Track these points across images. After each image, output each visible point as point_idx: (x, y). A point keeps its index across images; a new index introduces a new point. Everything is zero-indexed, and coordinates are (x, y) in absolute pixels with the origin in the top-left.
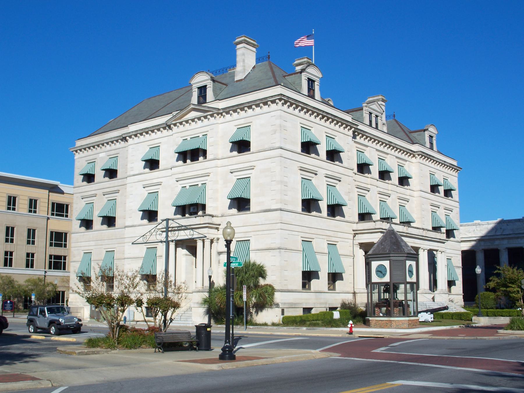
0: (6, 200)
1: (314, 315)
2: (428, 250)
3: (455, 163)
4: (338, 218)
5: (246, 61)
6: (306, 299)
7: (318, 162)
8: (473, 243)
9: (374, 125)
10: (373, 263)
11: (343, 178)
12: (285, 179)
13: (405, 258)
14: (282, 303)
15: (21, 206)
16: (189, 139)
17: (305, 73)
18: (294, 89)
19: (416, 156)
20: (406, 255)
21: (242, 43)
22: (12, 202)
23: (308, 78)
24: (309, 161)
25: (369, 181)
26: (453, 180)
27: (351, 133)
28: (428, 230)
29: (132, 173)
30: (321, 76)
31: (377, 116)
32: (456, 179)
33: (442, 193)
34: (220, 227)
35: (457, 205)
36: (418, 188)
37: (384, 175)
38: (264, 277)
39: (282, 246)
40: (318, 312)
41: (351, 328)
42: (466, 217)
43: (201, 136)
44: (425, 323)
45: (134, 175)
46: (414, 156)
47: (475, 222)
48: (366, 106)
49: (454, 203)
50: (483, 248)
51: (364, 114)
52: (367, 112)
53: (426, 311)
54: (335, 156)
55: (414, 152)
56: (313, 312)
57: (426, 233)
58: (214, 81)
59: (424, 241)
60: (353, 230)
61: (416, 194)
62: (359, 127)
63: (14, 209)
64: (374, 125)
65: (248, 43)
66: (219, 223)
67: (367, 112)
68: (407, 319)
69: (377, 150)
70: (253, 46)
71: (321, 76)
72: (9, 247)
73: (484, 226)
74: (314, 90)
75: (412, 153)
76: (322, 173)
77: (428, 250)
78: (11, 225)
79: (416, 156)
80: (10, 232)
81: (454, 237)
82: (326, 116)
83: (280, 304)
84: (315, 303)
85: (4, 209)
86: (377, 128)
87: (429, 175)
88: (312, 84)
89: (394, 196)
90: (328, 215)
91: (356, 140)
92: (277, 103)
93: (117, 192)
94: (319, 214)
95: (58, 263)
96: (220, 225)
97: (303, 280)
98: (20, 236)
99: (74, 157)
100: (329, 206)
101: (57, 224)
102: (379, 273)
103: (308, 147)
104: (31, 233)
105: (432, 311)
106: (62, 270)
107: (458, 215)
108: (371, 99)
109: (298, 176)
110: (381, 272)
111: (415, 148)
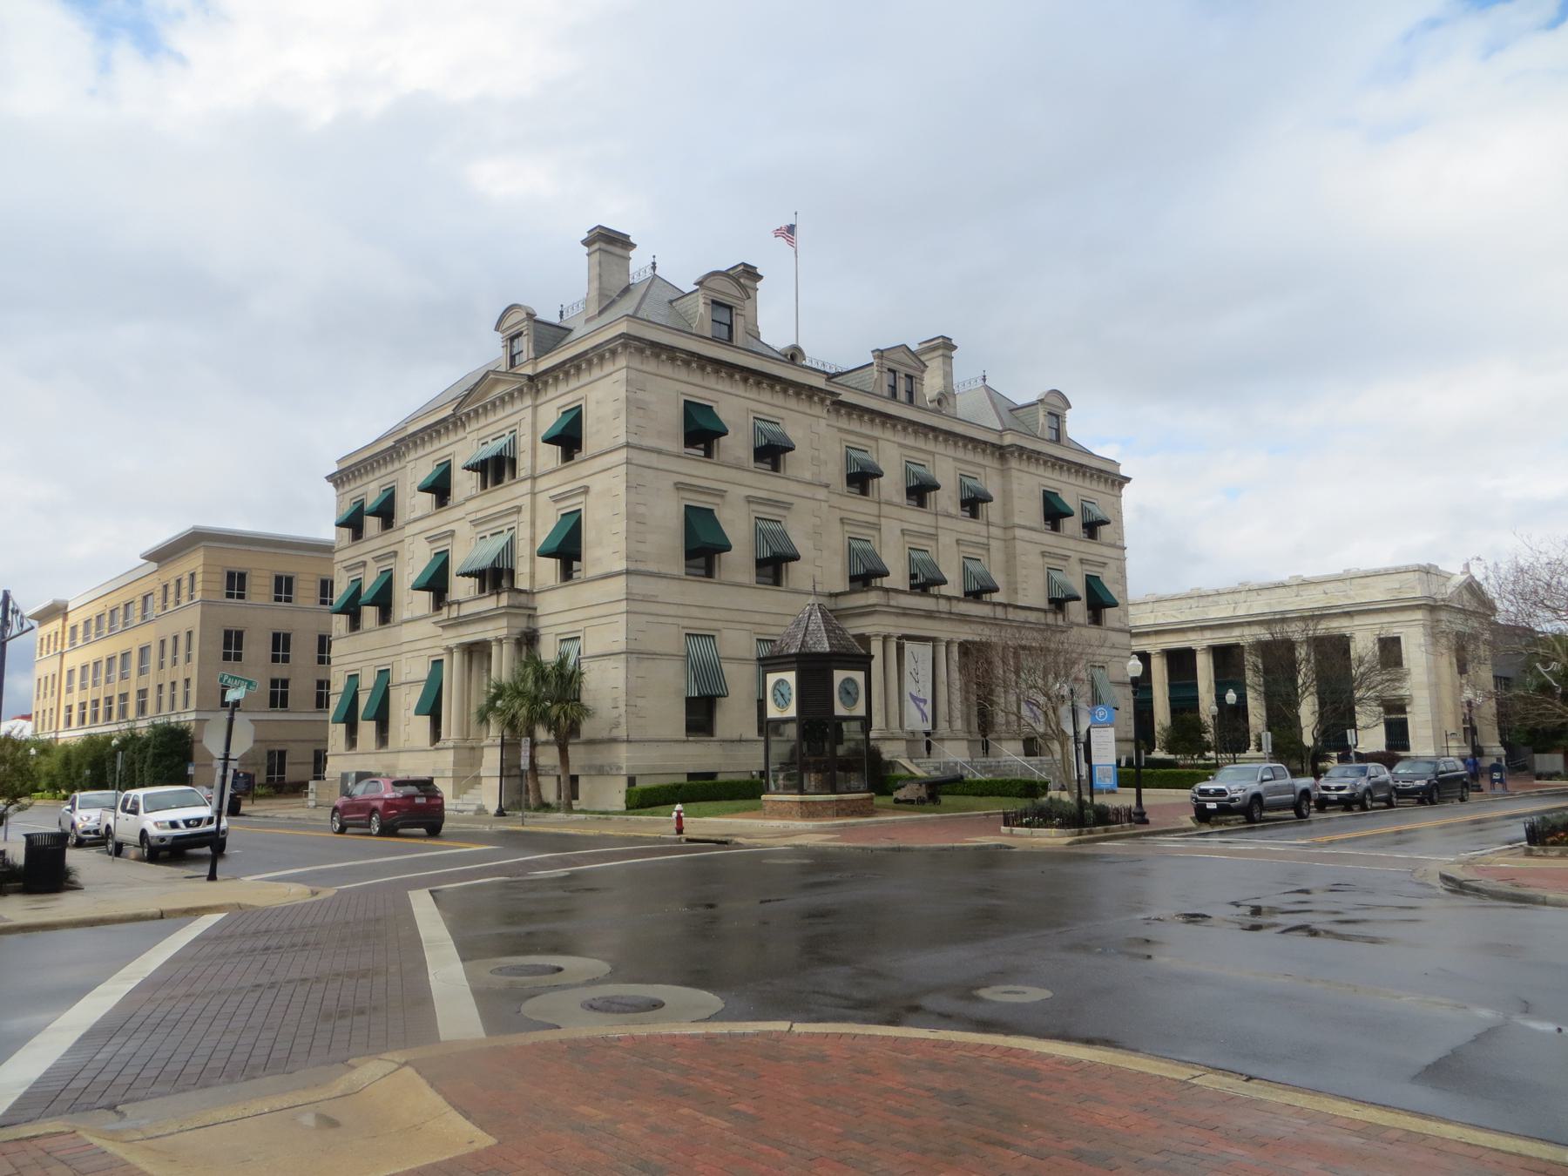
9: (902, 395)
10: (836, 673)
12: (641, 509)
29: (414, 516)
41: (679, 818)
43: (506, 432)
63: (288, 600)
64: (902, 395)
68: (798, 798)
72: (280, 671)
78: (282, 629)
86: (911, 400)
97: (1405, 721)
98: (257, 649)
104: (281, 644)
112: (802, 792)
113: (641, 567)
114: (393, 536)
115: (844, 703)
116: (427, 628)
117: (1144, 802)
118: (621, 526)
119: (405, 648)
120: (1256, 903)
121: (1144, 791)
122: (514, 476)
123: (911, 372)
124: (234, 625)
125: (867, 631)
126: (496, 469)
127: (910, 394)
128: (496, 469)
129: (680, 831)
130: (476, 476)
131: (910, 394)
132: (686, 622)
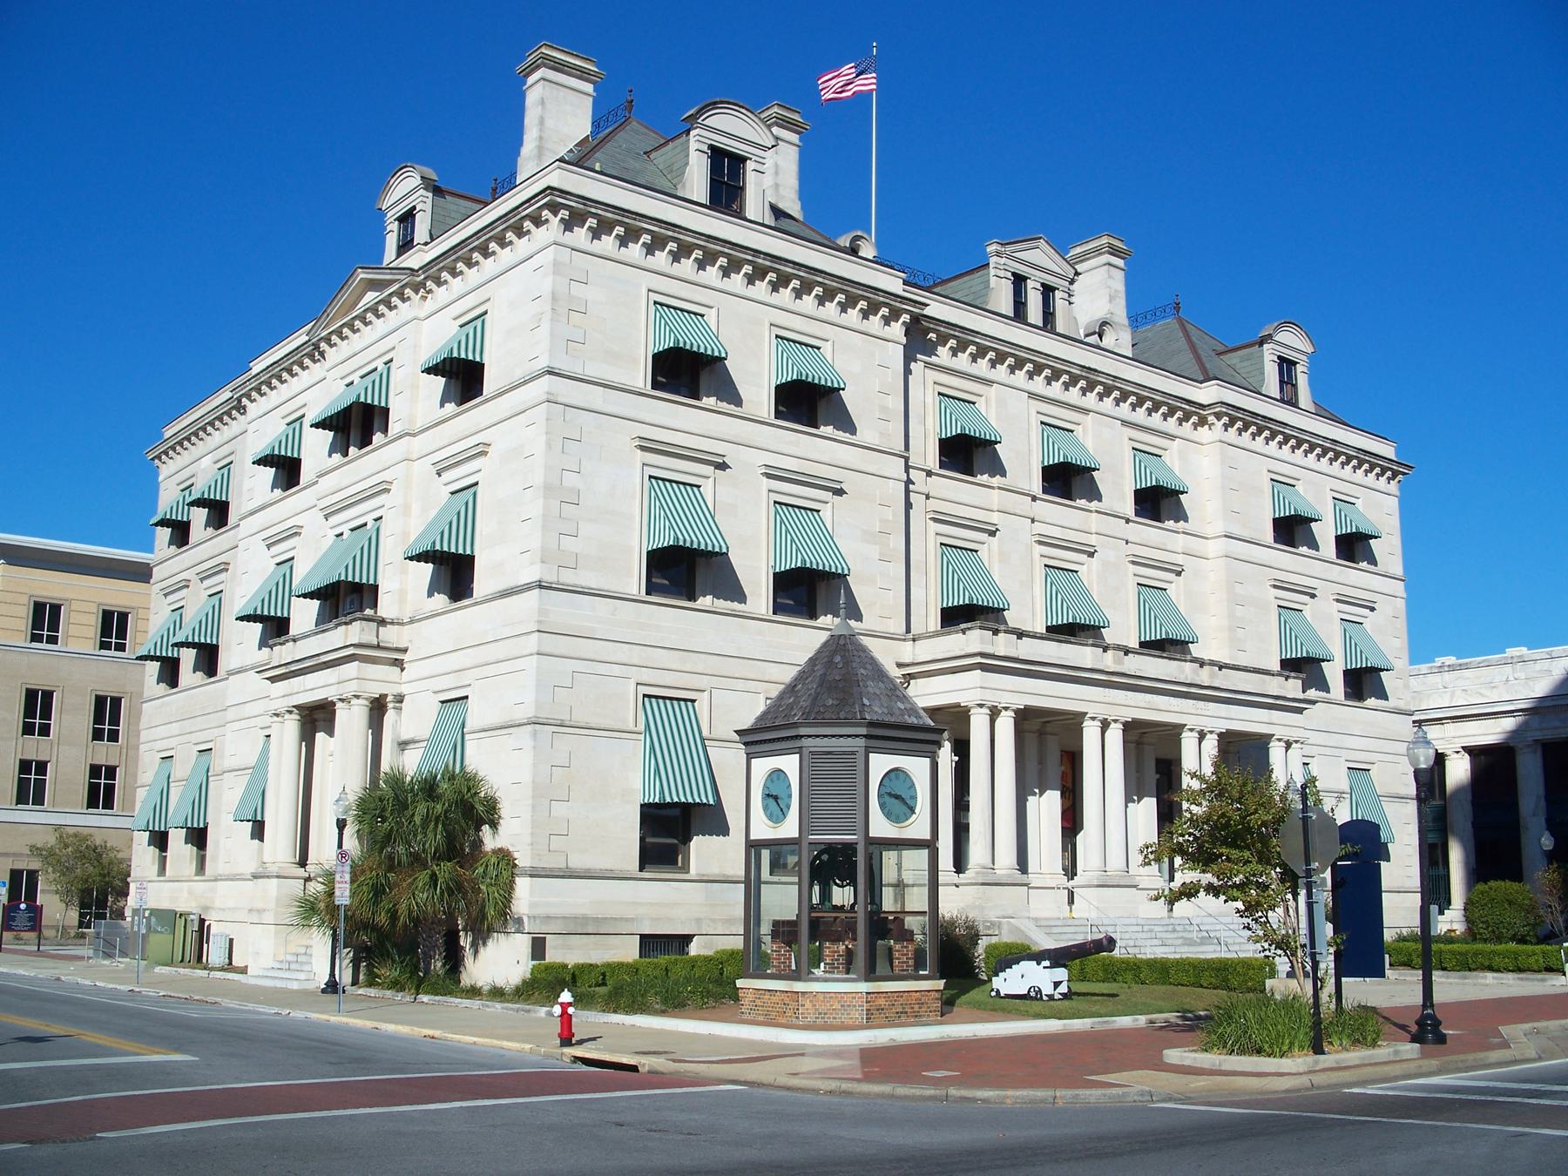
0: (25, 614)
1: (694, 962)
2: (1220, 735)
3: (1387, 450)
4: (1371, 702)
5: (549, 123)
6: (665, 903)
7: (1317, 566)
8: (1509, 724)
9: (1034, 312)
11: (849, 481)
12: (570, 480)
13: (861, 742)
14: (532, 918)
15: (73, 630)
16: (357, 380)
17: (697, 131)
18: (1246, 384)
19: (1211, 419)
20: (863, 731)
21: (538, 67)
22: (45, 619)
23: (711, 147)
24: (1289, 561)
25: (1094, 522)
26: (1378, 507)
27: (897, 330)
28: (1034, 636)
30: (1310, 349)
31: (1048, 290)
32: (1394, 503)
33: (1328, 548)
34: (406, 657)
35: (1399, 588)
36: (1220, 528)
37: (1066, 480)
38: (494, 825)
39: (544, 714)
40: (710, 953)
42: (1439, 631)
43: (379, 364)
44: (1029, 1001)
45: (252, 513)
46: (1203, 422)
47: (1512, 652)
48: (998, 254)
49: (1384, 583)
50: (1538, 735)
51: (993, 280)
52: (1002, 273)
53: (1038, 957)
54: (1299, 532)
55: (1202, 406)
56: (694, 949)
57: (1212, 675)
58: (437, 191)
59: (1149, 696)
60: (900, 665)
61: (1214, 548)
62: (927, 311)
63: (53, 640)
64: (1034, 312)
65: (559, 67)
66: (402, 646)
67: (1002, 273)
68: (864, 987)
69: (1033, 396)
70: (582, 75)
71: (1310, 349)
72: (34, 748)
73: (1538, 666)
74: (1295, 386)
75: (1194, 413)
76: (1326, 592)
77: (1220, 735)
78: (110, 691)
79: (1211, 419)
80: (37, 708)
81: (1383, 695)
82: (1331, 450)
83: (525, 920)
84: (698, 920)
85: (22, 640)
87: (1267, 485)
88: (1289, 371)
89: (1110, 553)
90: (1347, 696)
91: (934, 359)
92: (1210, 426)
93: (223, 568)
94: (736, 606)
95: (101, 791)
96: (405, 650)
99: (157, 475)
100: (1347, 673)
101: (108, 673)
102: (771, 802)
103: (1292, 530)
105: (1058, 958)
106: (101, 811)
107: (1401, 624)
108: (1078, 250)
109: (632, 470)
110: (776, 798)
111: (1207, 393)
112: (871, 974)
113: (568, 578)
114: (225, 538)
115: (888, 815)
116: (257, 683)
117: (1438, 997)
118: (534, 507)
119: (231, 714)
120: (927, 453)
121: (1437, 976)
122: (385, 431)
123: (1051, 281)
124: (40, 683)
125: (963, 699)
126: (357, 424)
127: (1048, 315)
128: (357, 424)
129: (567, 1039)
130: (328, 436)
131: (1048, 315)
132: (647, 675)
